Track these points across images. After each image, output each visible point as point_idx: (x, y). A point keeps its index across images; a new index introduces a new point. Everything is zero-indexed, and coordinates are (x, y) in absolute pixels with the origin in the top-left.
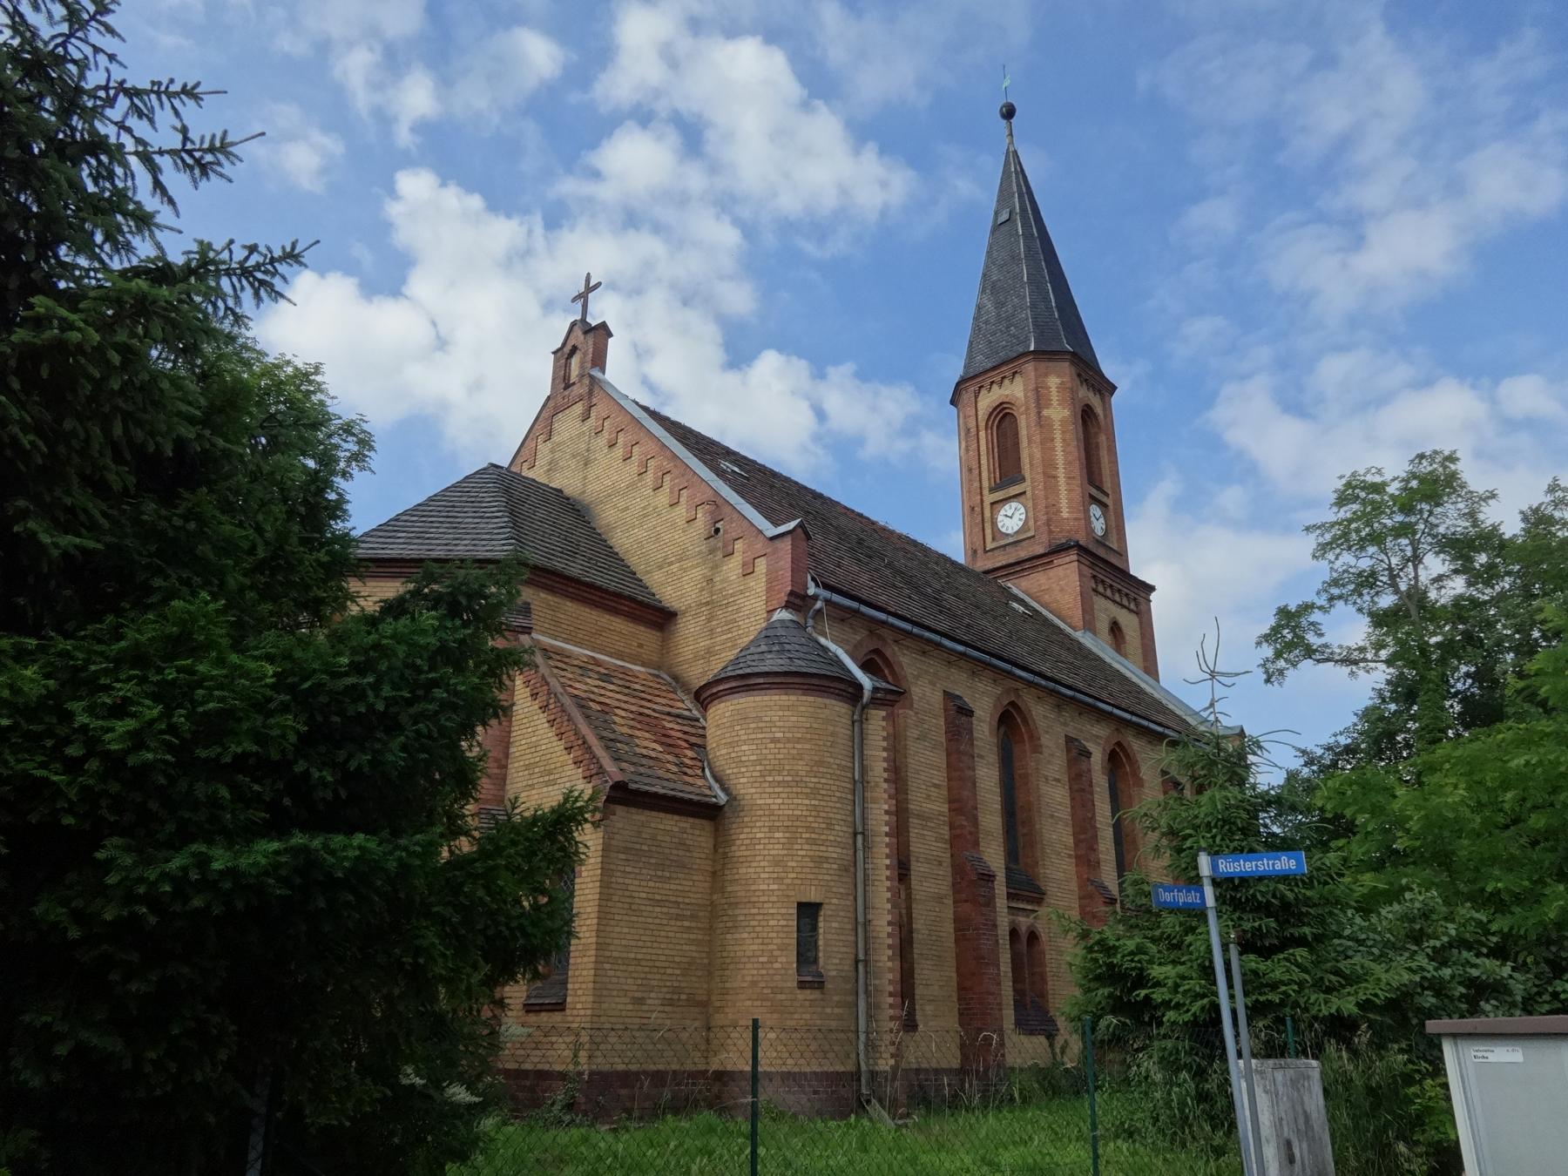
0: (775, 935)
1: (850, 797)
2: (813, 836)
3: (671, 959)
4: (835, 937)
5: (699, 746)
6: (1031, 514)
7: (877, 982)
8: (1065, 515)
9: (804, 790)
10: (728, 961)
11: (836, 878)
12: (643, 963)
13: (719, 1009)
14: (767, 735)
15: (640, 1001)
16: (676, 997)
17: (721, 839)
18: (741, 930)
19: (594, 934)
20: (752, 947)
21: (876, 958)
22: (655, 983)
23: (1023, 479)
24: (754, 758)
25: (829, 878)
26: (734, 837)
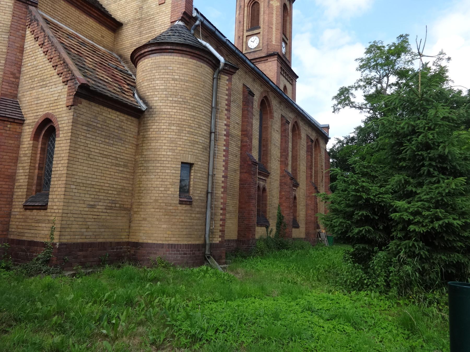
0: (169, 177)
2: (191, 130)
3: (111, 186)
4: (199, 181)
6: (261, 41)
7: (216, 203)
8: (274, 43)
9: (188, 107)
10: (143, 189)
11: (201, 152)
13: (136, 212)
14: (170, 76)
15: (93, 206)
16: (113, 205)
17: (142, 128)
18: (151, 174)
19: (65, 168)
20: (156, 183)
21: (216, 192)
22: (102, 197)
23: (260, 28)
24: (163, 87)
25: (197, 152)
26: (149, 127)
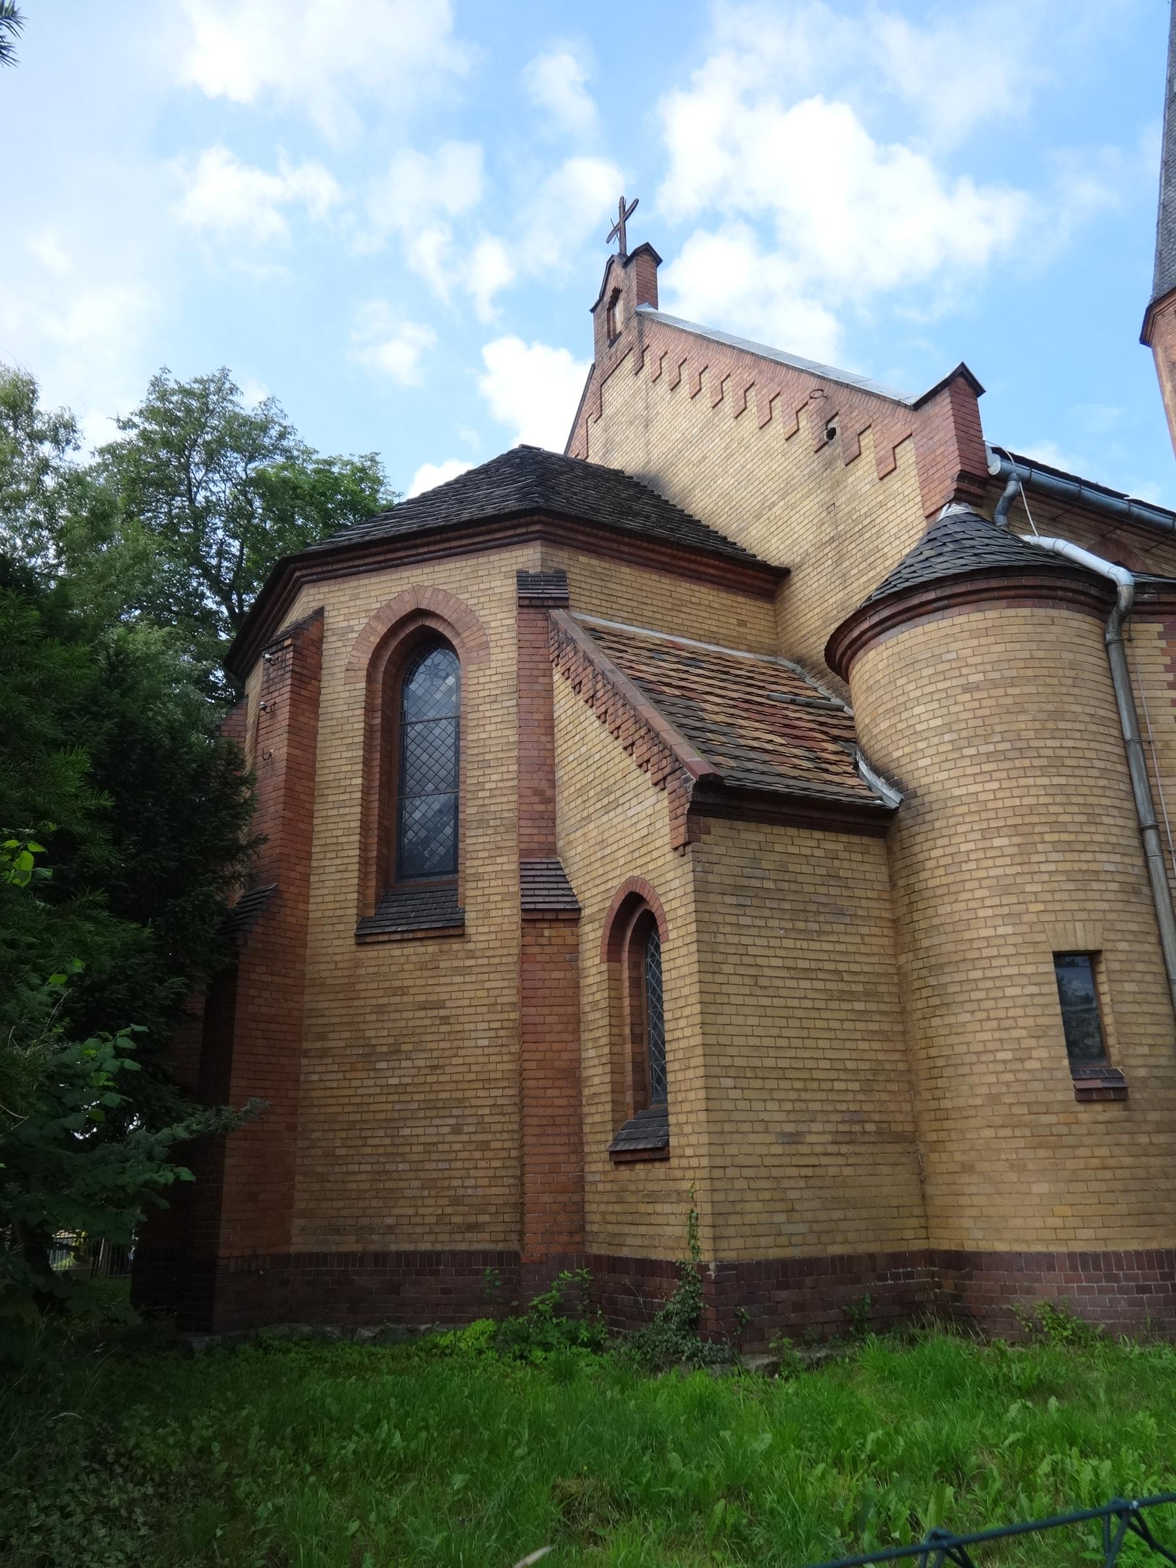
1: (1120, 768)
2: (1065, 837)
3: (838, 1065)
5: (847, 740)
9: (1036, 762)
10: (940, 1062)
11: (1119, 906)
12: (790, 1074)
13: (934, 1146)
14: (955, 682)
15: (793, 1139)
16: (857, 1128)
17: (899, 865)
19: (698, 1030)
20: (981, 1036)
22: (816, 1106)
24: (939, 722)
25: (1105, 906)
26: (921, 857)
